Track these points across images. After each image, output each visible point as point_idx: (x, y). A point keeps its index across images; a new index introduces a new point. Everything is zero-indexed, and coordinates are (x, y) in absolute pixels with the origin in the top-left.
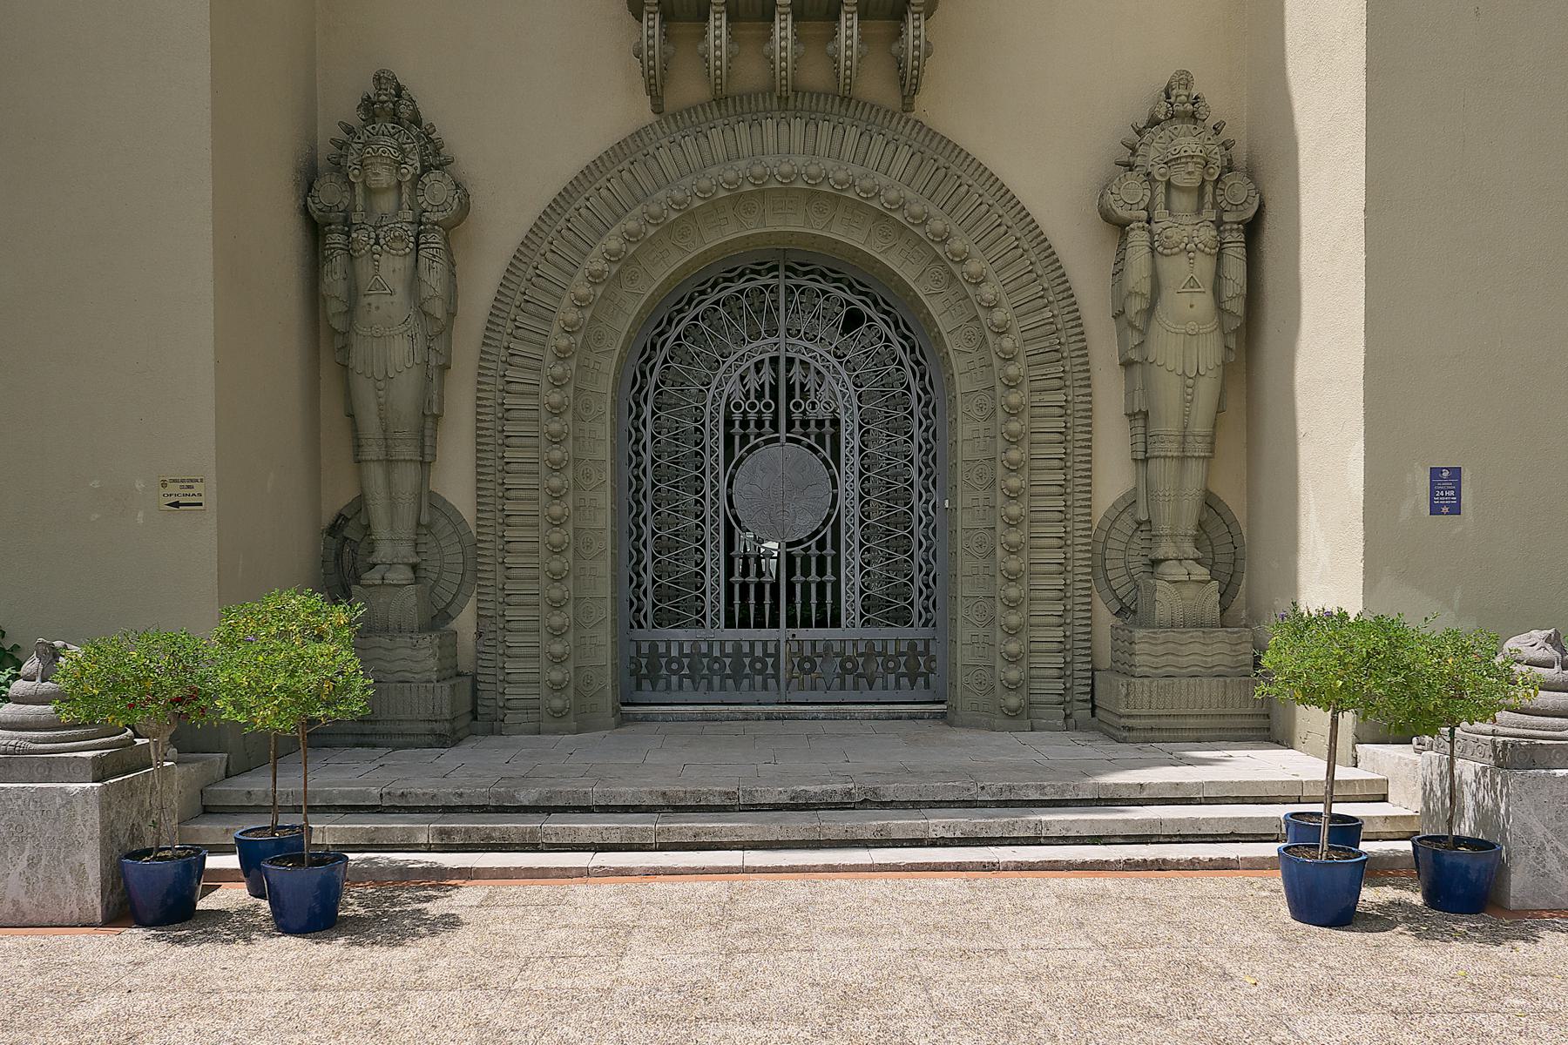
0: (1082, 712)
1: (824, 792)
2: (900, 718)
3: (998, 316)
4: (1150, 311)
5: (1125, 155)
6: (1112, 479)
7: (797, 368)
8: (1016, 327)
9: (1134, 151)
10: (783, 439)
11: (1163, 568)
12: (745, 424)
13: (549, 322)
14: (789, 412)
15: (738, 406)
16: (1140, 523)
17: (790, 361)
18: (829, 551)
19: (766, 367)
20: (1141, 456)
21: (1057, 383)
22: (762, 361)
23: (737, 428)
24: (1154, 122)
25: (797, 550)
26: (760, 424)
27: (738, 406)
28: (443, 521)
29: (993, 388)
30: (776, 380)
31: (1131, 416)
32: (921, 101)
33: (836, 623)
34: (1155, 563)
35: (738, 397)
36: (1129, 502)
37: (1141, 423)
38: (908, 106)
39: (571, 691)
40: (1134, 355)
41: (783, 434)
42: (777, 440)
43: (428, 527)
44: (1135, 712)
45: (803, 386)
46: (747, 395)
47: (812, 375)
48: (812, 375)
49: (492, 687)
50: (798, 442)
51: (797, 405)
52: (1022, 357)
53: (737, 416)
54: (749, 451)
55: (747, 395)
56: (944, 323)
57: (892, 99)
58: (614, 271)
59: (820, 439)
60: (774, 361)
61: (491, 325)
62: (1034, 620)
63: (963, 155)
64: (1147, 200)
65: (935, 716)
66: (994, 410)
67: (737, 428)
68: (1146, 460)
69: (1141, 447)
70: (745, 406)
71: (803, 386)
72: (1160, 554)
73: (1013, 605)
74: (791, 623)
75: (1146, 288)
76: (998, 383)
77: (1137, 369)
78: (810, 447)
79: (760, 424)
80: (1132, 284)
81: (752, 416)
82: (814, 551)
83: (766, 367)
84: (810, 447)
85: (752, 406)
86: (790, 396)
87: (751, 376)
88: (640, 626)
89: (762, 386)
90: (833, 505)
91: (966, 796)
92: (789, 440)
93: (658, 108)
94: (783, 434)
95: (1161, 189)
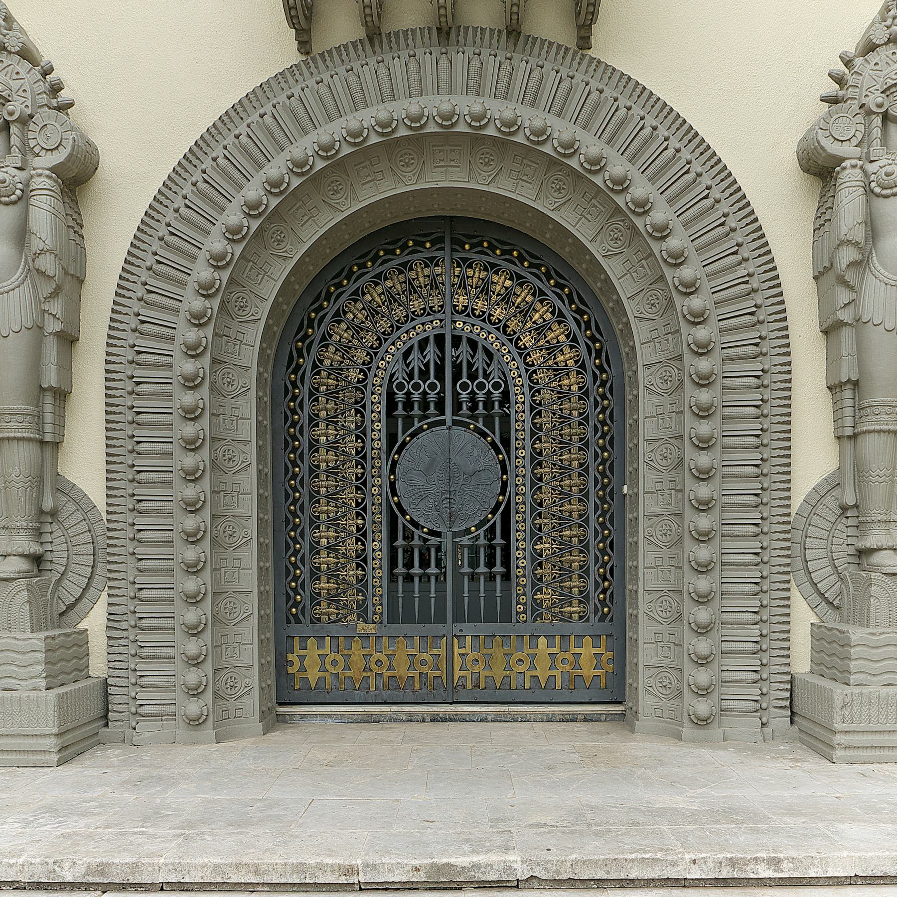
0: (780, 720)
1: (475, 866)
2: (574, 720)
3: (687, 272)
4: (860, 265)
5: (832, 88)
6: (814, 458)
7: (464, 347)
8: (706, 286)
9: (839, 80)
10: (449, 423)
11: (877, 558)
12: (408, 404)
13: (182, 284)
14: (456, 394)
15: (401, 386)
16: (844, 509)
17: (457, 341)
18: (499, 541)
19: (431, 348)
20: (849, 432)
21: (752, 349)
22: (426, 340)
23: (400, 411)
24: (870, 48)
25: (465, 540)
26: (425, 405)
27: (401, 386)
28: (71, 507)
29: (680, 358)
30: (442, 359)
31: (833, 388)
32: (599, 33)
33: (506, 618)
34: (863, 553)
35: (400, 377)
36: (833, 484)
37: (848, 394)
38: (584, 42)
39: (209, 694)
40: (845, 316)
41: (448, 416)
42: (443, 423)
43: (54, 513)
44: (852, 727)
45: (470, 365)
46: (411, 376)
47: (480, 355)
48: (480, 355)
49: (123, 691)
50: (466, 425)
51: (464, 387)
52: (713, 320)
53: (400, 397)
54: (412, 436)
55: (411, 376)
56: (624, 288)
57: (565, 36)
58: (254, 228)
59: (489, 421)
60: (440, 340)
61: (121, 291)
62: (725, 617)
63: (646, 94)
64: (859, 136)
65: (611, 718)
66: (681, 381)
67: (400, 411)
68: (854, 437)
69: (849, 421)
70: (408, 387)
71: (470, 365)
72: (870, 542)
73: (703, 599)
74: (455, 621)
75: (859, 235)
76: (686, 350)
77: (846, 336)
78: (477, 430)
79: (425, 405)
80: (844, 230)
81: (416, 396)
82: (482, 541)
83: (431, 348)
84: (477, 430)
85: (416, 387)
86: (457, 376)
87: (415, 354)
88: (298, 621)
89: (427, 365)
90: (503, 492)
91: (672, 873)
92: (455, 423)
93: (304, 44)
94: (448, 416)
95: (878, 121)
